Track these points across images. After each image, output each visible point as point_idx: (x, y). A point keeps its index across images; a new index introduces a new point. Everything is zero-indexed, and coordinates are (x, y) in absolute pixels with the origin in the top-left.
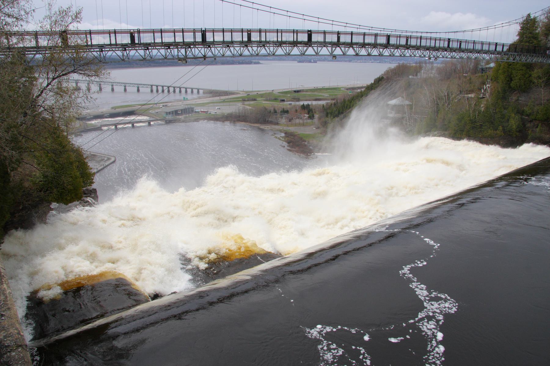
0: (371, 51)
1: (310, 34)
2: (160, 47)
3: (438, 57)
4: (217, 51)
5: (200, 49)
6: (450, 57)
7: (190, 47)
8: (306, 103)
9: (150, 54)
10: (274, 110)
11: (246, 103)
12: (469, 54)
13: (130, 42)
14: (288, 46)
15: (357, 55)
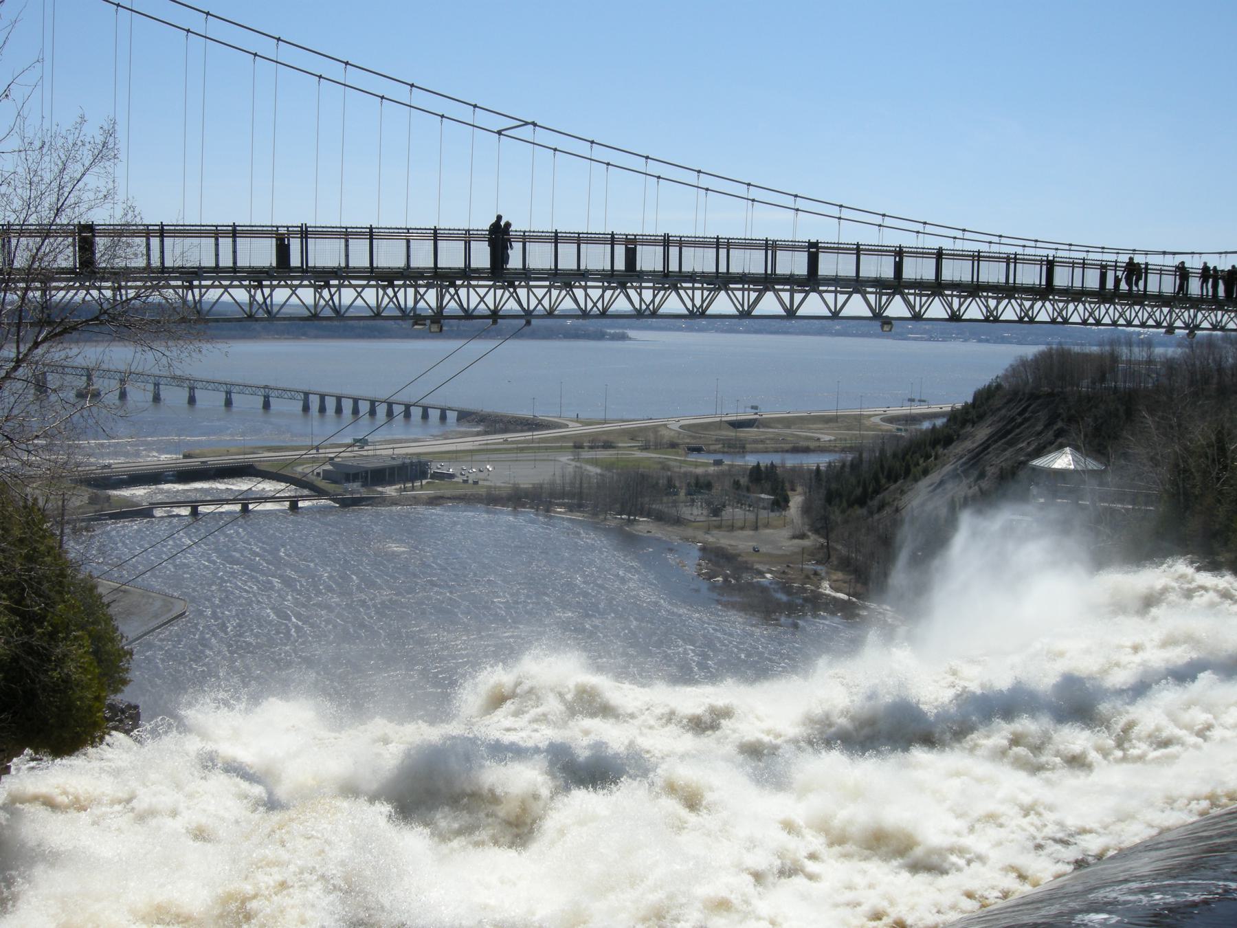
0: (961, 305)
1: (813, 251)
2: (365, 282)
3: (1197, 327)
4: (535, 297)
7: (453, 285)
8: (765, 460)
9: (332, 298)
10: (670, 480)
11: (586, 454)
13: (274, 264)
15: (917, 317)
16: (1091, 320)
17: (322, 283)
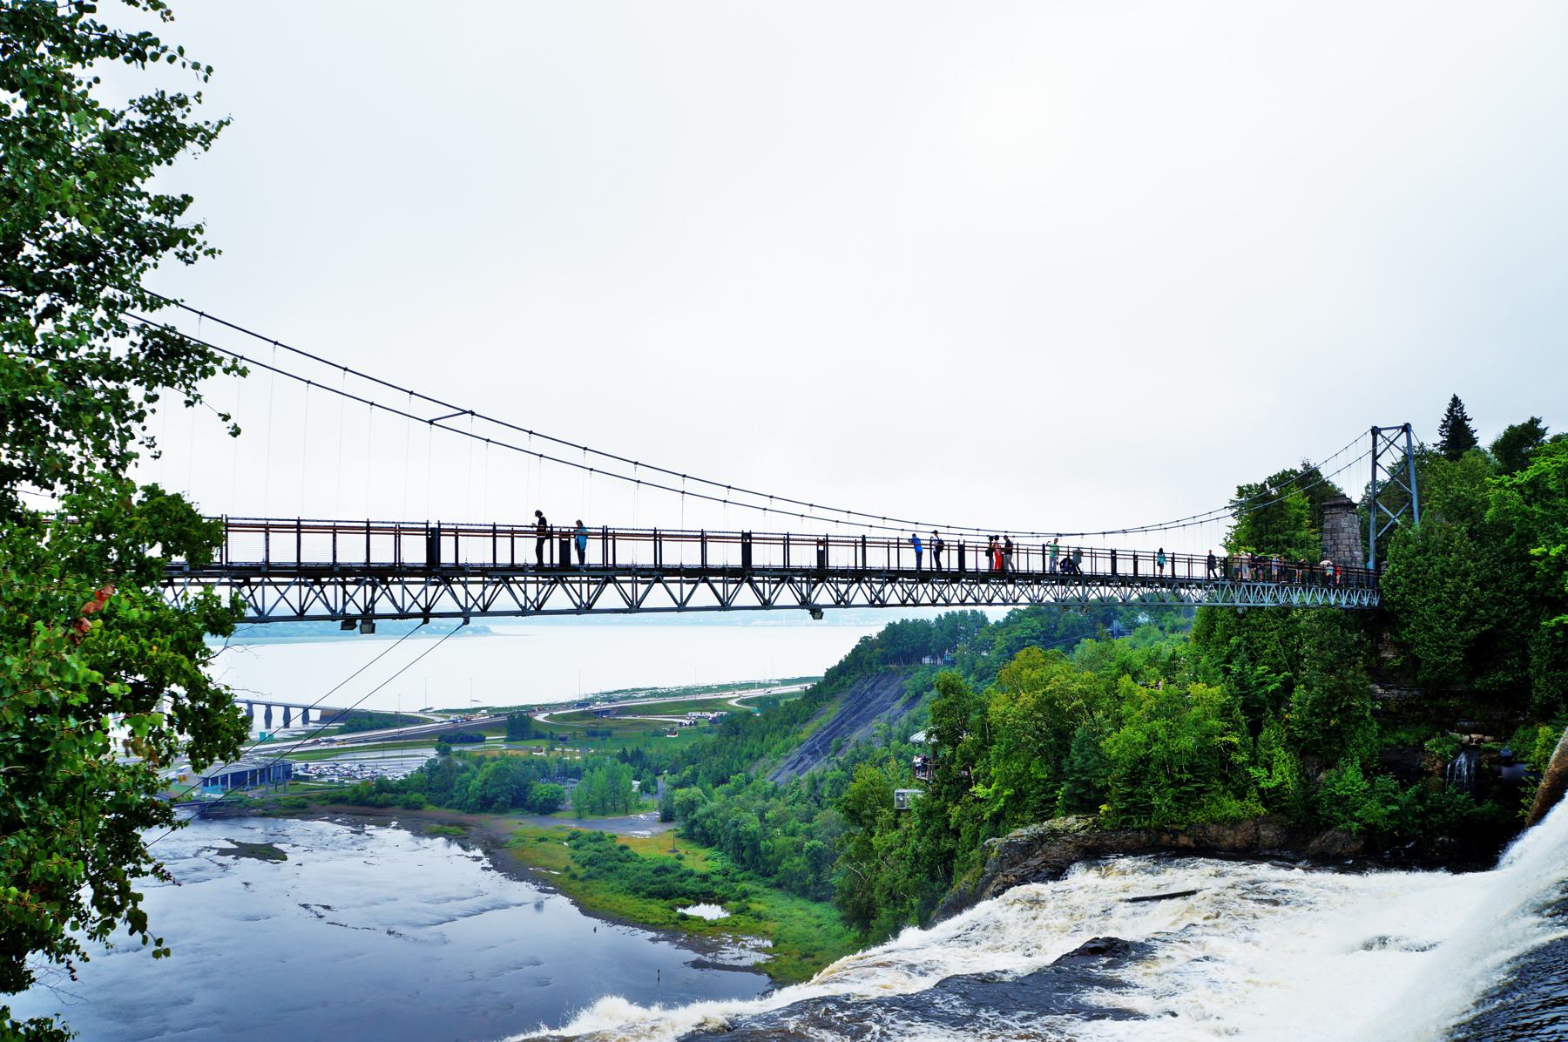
5: (282, 588)
12: (1056, 587)
14: (584, 582)
16: (910, 601)
17: (241, 581)
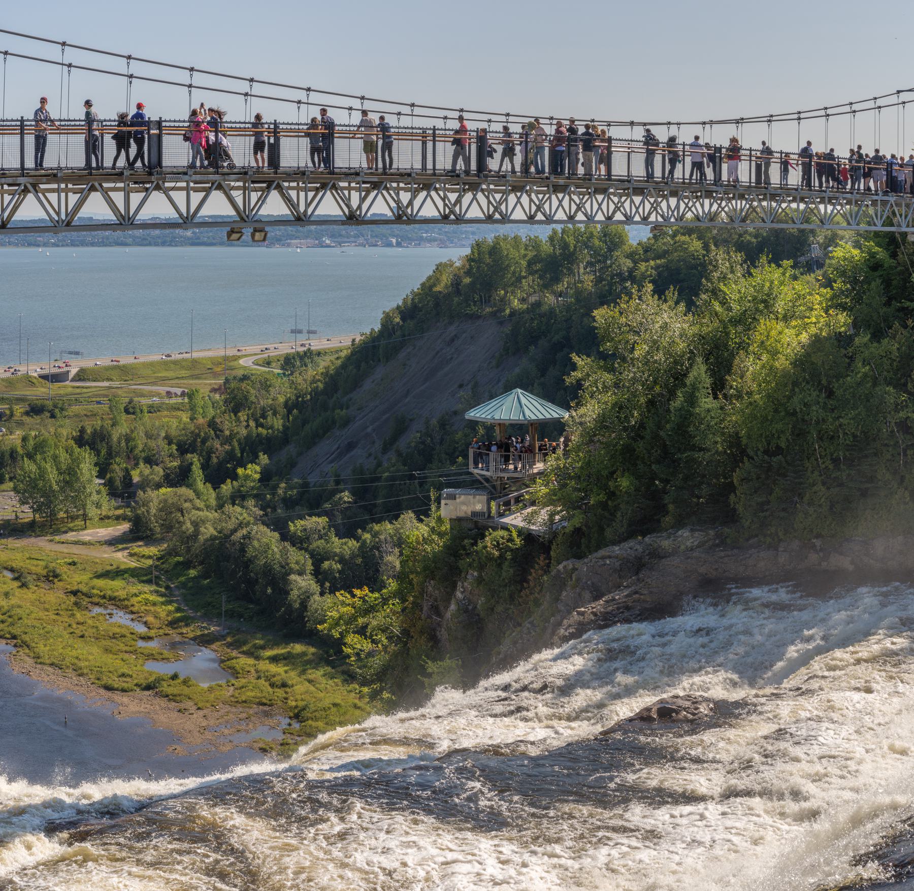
0: (363, 200)
6: (623, 219)
12: (734, 202)
14: (354, 188)
